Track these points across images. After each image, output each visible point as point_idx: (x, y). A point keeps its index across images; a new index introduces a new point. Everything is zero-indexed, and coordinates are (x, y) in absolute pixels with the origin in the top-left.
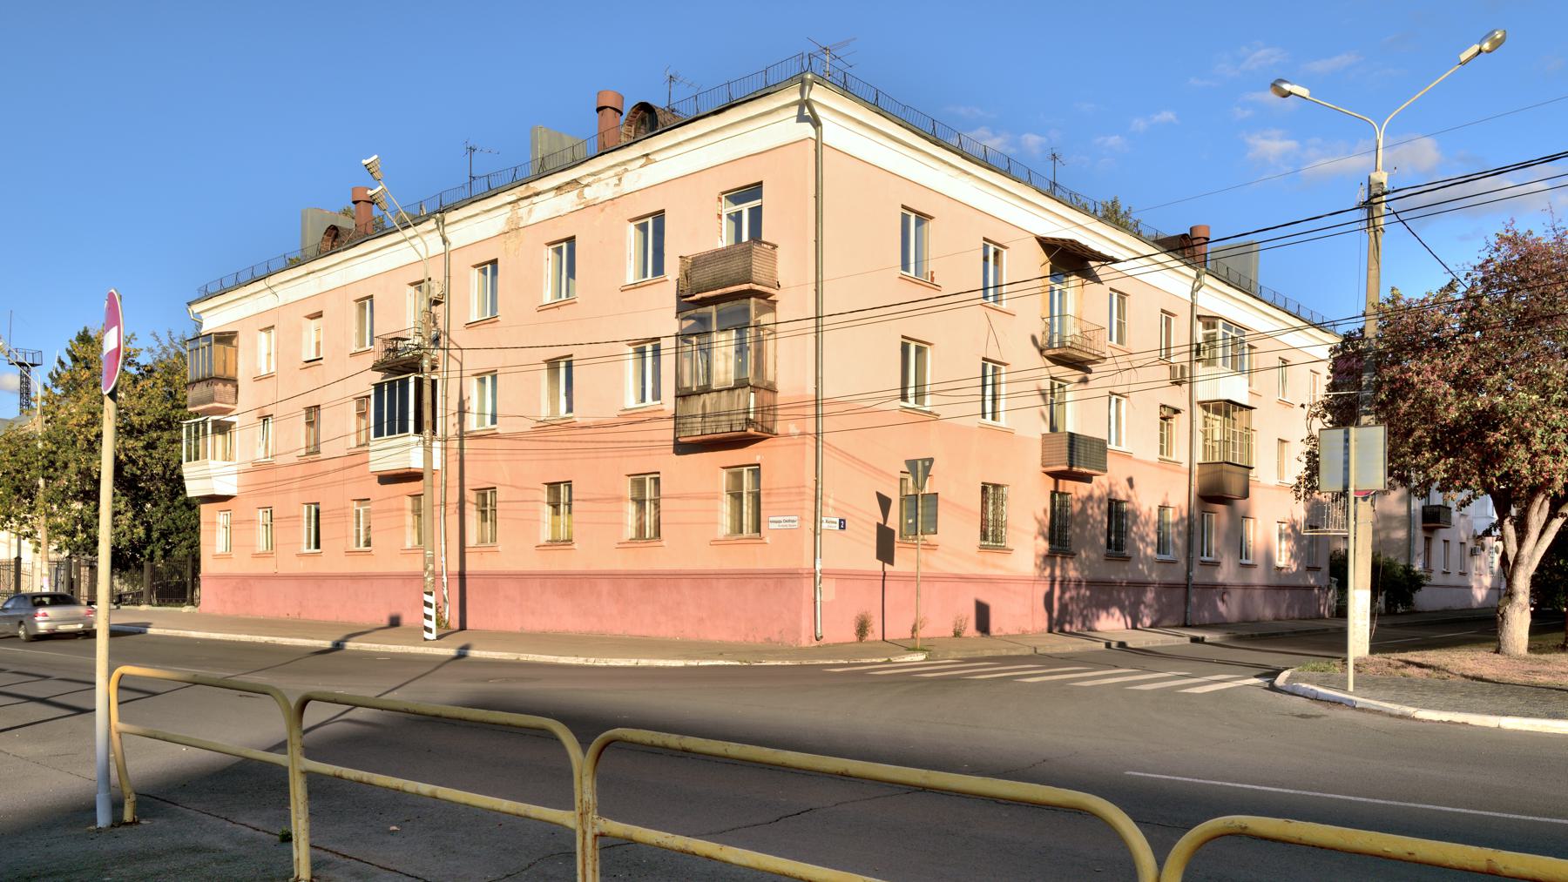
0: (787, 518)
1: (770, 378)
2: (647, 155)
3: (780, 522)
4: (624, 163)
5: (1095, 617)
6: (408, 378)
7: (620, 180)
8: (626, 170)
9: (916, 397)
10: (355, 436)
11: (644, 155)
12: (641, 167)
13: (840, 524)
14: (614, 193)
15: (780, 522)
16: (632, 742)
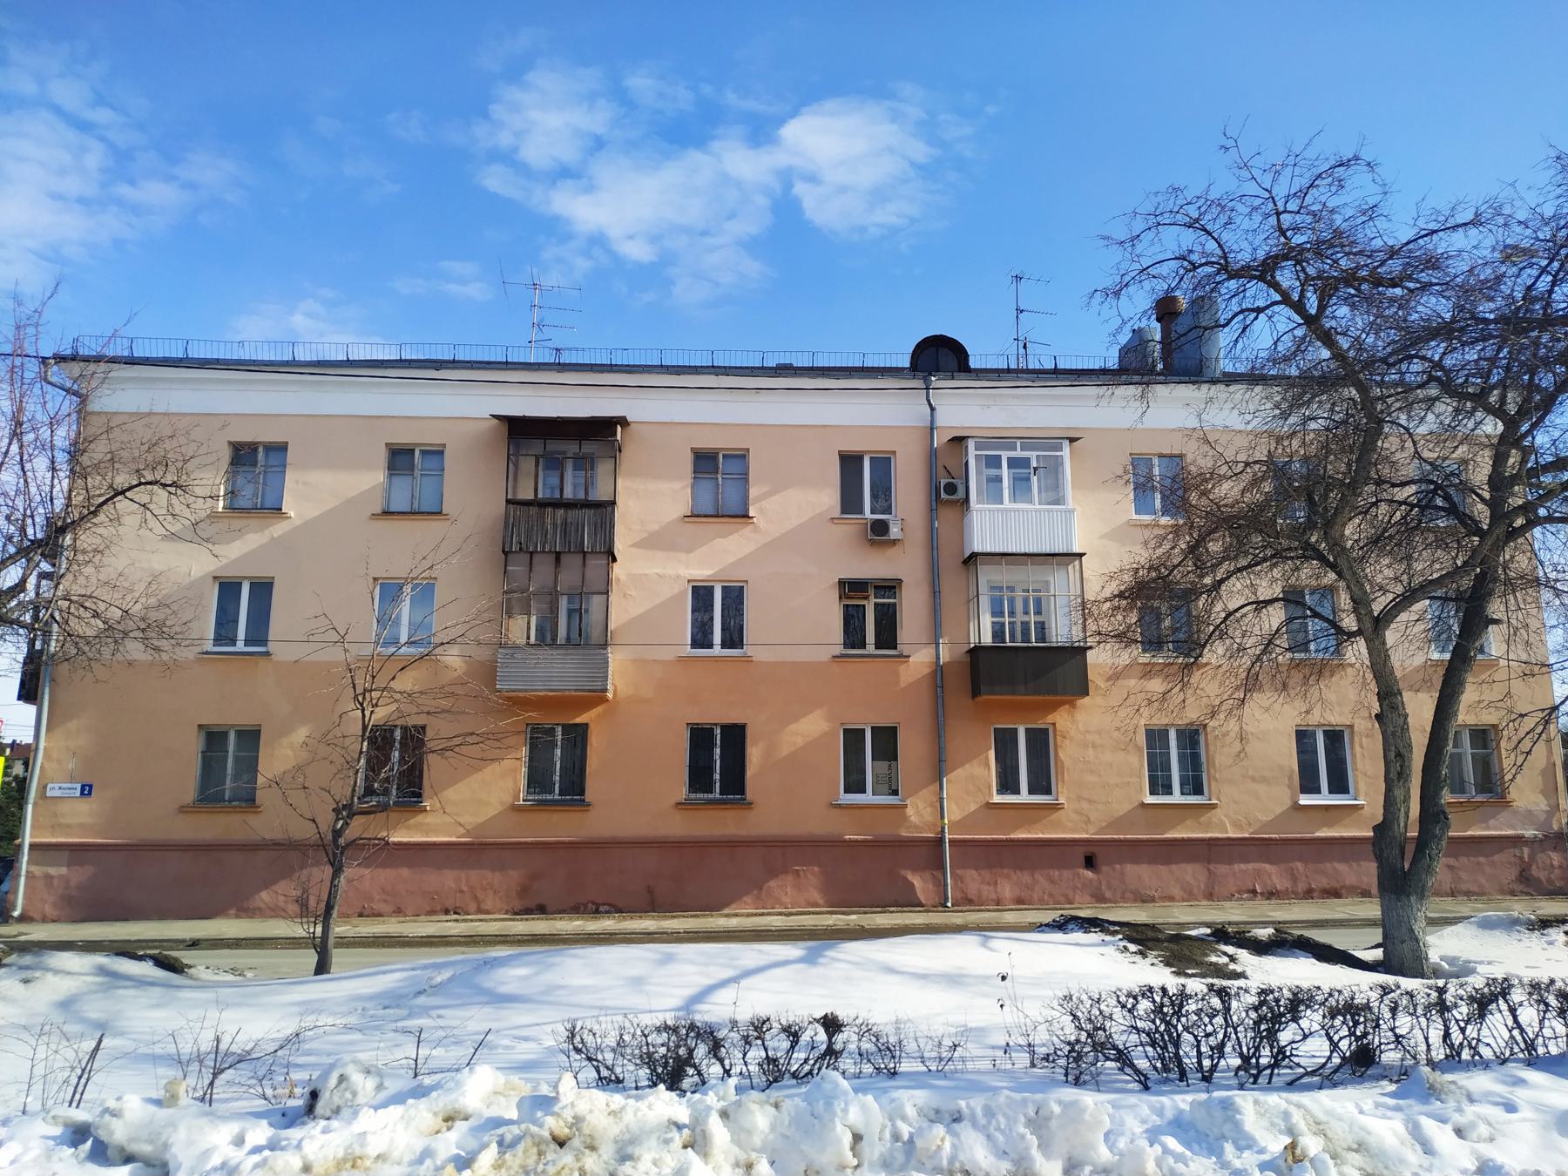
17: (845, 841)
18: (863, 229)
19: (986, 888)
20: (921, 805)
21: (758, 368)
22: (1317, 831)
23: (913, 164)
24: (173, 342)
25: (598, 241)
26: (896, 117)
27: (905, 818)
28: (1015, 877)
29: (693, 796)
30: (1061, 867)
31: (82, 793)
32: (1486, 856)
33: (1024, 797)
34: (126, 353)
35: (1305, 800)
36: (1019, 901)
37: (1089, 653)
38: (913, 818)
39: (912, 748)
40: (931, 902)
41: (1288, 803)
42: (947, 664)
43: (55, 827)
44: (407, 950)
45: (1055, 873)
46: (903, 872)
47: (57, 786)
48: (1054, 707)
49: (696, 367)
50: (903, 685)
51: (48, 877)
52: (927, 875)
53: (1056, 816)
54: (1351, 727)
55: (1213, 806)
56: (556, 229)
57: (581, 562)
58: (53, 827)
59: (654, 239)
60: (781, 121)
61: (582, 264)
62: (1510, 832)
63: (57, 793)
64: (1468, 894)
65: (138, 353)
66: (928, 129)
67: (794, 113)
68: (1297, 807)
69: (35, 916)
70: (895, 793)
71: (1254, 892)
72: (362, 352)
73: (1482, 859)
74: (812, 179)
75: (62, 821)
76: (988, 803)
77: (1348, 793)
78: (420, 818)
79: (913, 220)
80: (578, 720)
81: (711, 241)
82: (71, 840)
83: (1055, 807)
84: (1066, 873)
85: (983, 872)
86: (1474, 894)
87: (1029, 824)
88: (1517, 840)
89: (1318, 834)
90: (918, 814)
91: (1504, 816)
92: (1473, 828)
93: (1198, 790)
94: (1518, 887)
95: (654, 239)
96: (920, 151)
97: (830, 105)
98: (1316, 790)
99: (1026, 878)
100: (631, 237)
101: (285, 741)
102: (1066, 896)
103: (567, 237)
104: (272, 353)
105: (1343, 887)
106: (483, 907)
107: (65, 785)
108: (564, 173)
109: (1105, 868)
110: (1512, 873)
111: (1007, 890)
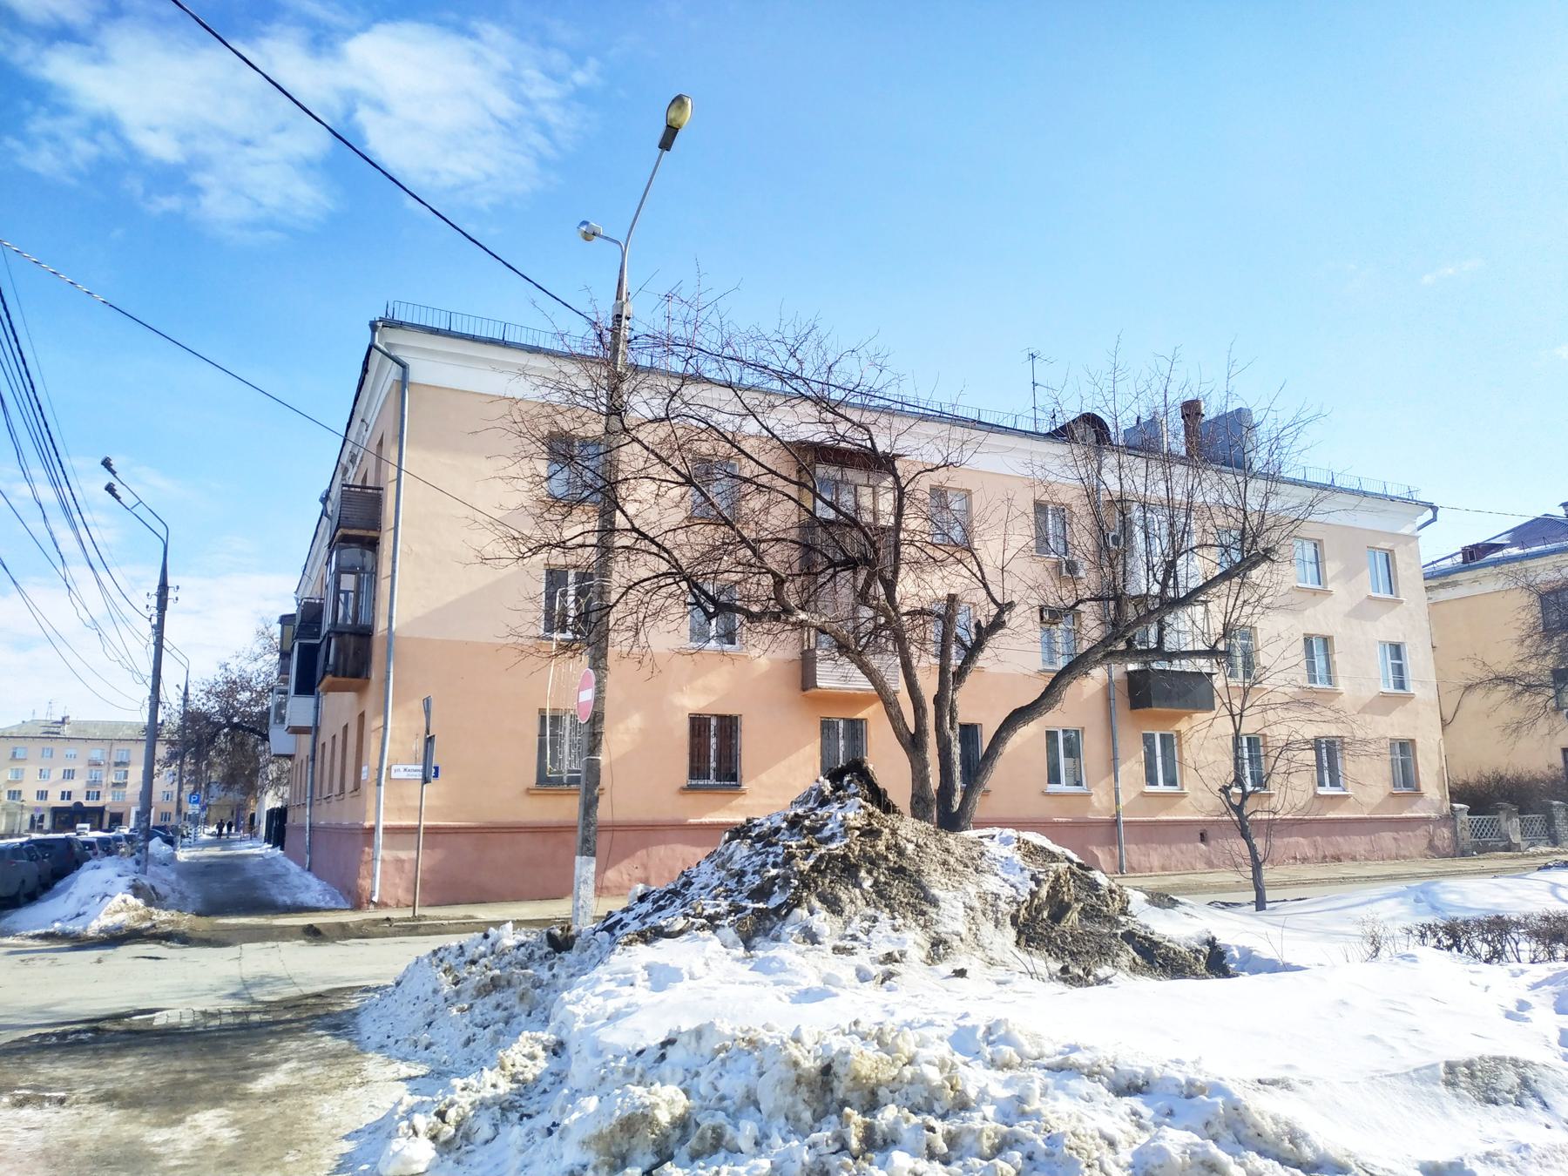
16: (707, 825)
17: (690, 825)
18: (434, 173)
19: (1142, 858)
20: (1101, 794)
21: (1032, 433)
23: (494, 117)
24: (459, 316)
25: (103, 124)
26: (478, 58)
27: (1090, 804)
28: (1159, 850)
29: (694, 782)
30: (1186, 842)
32: (1412, 831)
33: (1161, 788)
34: (1301, 478)
36: (1163, 868)
38: (1096, 804)
39: (1093, 748)
40: (1109, 870)
41: (1311, 793)
42: (1117, 681)
43: (401, 811)
45: (1184, 847)
46: (1090, 848)
47: (402, 768)
48: (1178, 718)
49: (1026, 432)
50: (1085, 697)
51: (400, 861)
52: (1106, 849)
53: (1184, 802)
56: (42, 95)
58: (399, 810)
59: (183, 137)
60: (350, 34)
61: (83, 150)
62: (1423, 815)
63: (403, 775)
64: (1404, 857)
66: (511, 81)
67: (365, 28)
68: (1317, 796)
69: (389, 902)
70: (1078, 783)
71: (1295, 858)
72: (518, 335)
73: (1410, 833)
74: (380, 106)
77: (1176, 785)
78: (740, 800)
79: (489, 177)
80: (859, 716)
81: (251, 152)
84: (1191, 847)
85: (1141, 846)
86: (1408, 857)
87: (1167, 808)
88: (1426, 820)
89: (1328, 816)
90: (1099, 804)
91: (1420, 802)
93: (1172, 782)
94: (1429, 853)
95: (183, 137)
96: (501, 103)
97: (409, 29)
98: (1058, 781)
99: (1166, 850)
100: (153, 129)
101: (621, 727)
102: (1191, 864)
103: (61, 110)
105: (1342, 854)
107: (410, 767)
108: (60, 34)
109: (1213, 843)
110: (1425, 843)
111: (1155, 860)
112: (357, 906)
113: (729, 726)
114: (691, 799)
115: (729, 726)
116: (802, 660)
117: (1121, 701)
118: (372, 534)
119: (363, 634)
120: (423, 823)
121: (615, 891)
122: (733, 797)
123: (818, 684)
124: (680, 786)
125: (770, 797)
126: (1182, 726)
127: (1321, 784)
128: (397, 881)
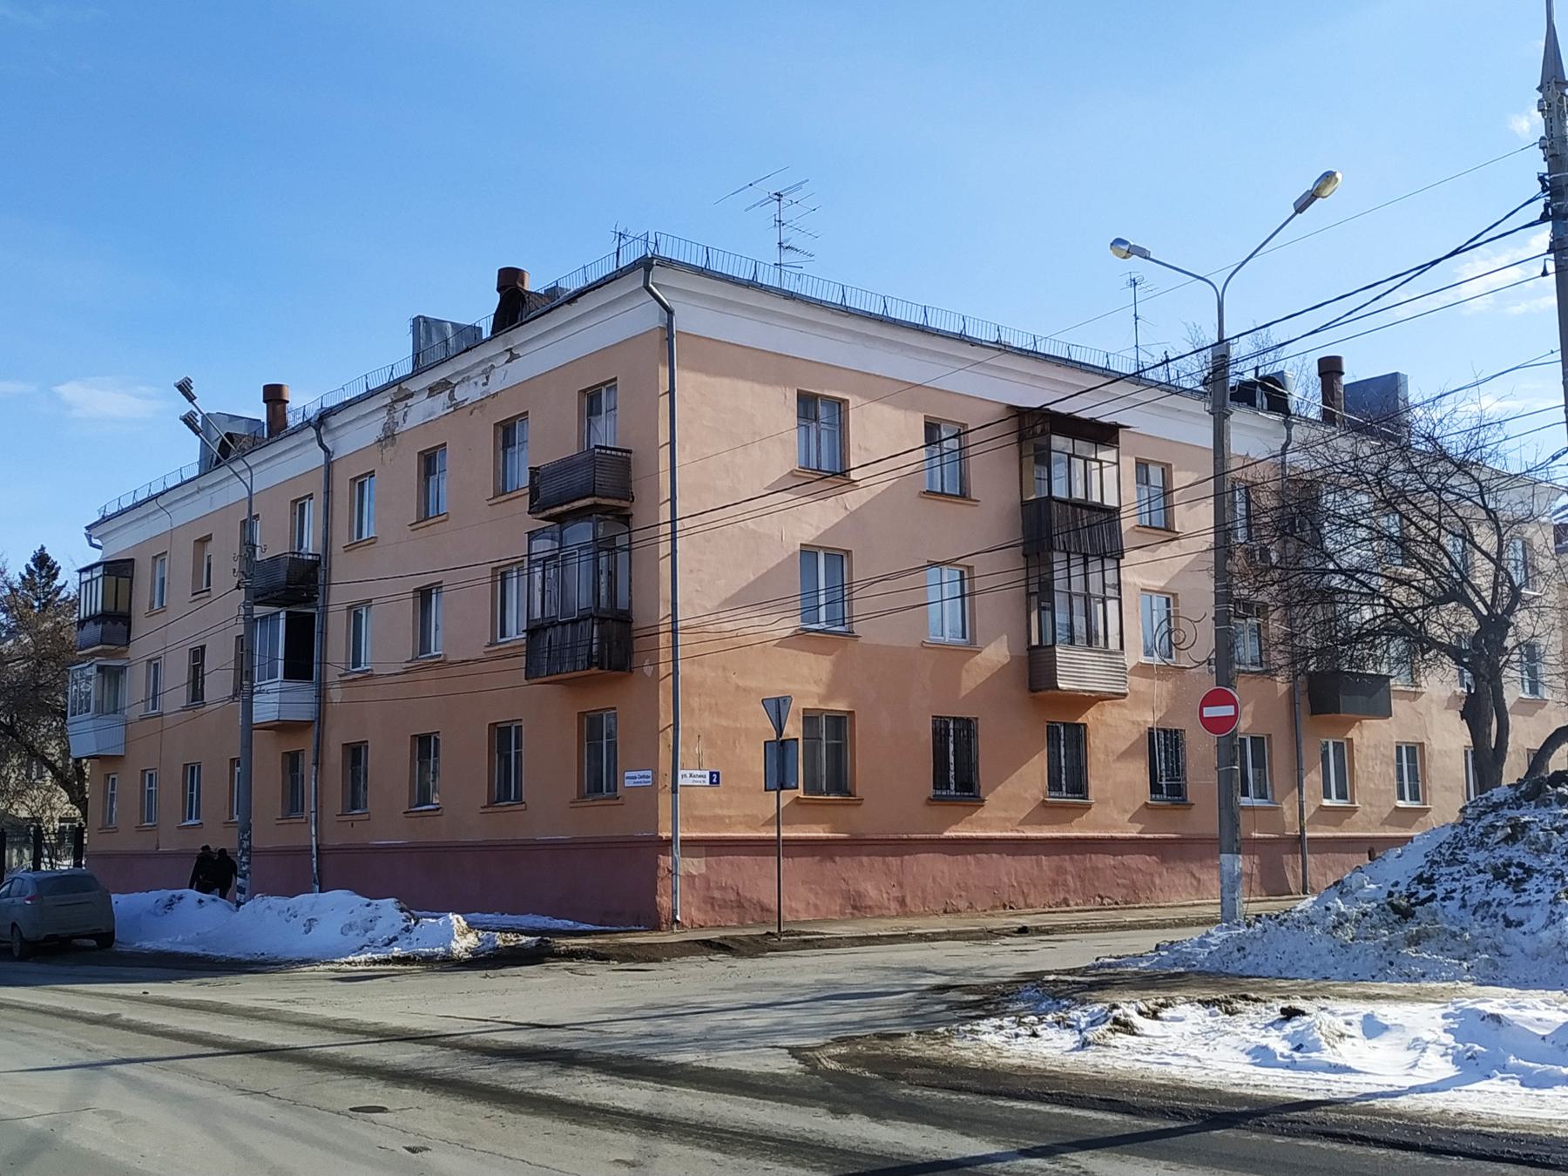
0: (642, 773)
1: (622, 604)
2: (510, 350)
3: (635, 778)
4: (489, 359)
5: (685, 1068)
6: (278, 613)
7: (487, 378)
8: (492, 366)
9: (1122, 550)
10: (1147, 515)
11: (507, 350)
12: (507, 362)
13: (711, 778)
14: (482, 394)
15: (635, 778)
16: (953, 839)
22: (945, 830)
29: (938, 793)
31: (711, 782)
35: (1326, 802)
37: (1392, 682)
44: (1150, 931)
47: (687, 773)
54: (1422, 745)
55: (1428, 810)
57: (997, 544)
65: (716, 266)
75: (696, 813)
76: (1321, 806)
77: (1346, 798)
78: (980, 813)
82: (694, 835)
83: (1355, 810)
89: (947, 834)
92: (954, 827)
104: (814, 292)
106: (1030, 901)
107: (695, 772)
112: (656, 927)
113: (966, 727)
114: (937, 812)
115: (966, 727)
116: (1029, 657)
117: (1304, 702)
118: (624, 504)
119: (624, 619)
120: (679, 835)
121: (877, 912)
122: (973, 809)
123: (1060, 685)
124: (925, 798)
125: (1006, 811)
126: (1353, 734)
127: (1327, 796)
128: (690, 898)
